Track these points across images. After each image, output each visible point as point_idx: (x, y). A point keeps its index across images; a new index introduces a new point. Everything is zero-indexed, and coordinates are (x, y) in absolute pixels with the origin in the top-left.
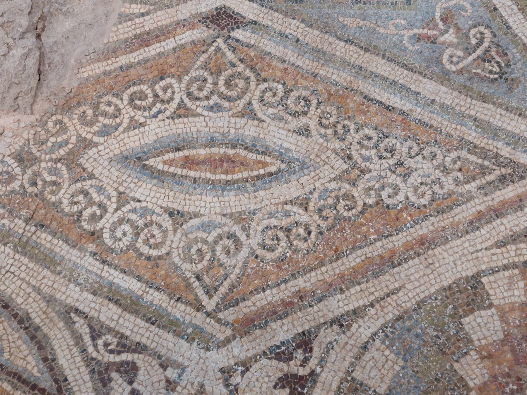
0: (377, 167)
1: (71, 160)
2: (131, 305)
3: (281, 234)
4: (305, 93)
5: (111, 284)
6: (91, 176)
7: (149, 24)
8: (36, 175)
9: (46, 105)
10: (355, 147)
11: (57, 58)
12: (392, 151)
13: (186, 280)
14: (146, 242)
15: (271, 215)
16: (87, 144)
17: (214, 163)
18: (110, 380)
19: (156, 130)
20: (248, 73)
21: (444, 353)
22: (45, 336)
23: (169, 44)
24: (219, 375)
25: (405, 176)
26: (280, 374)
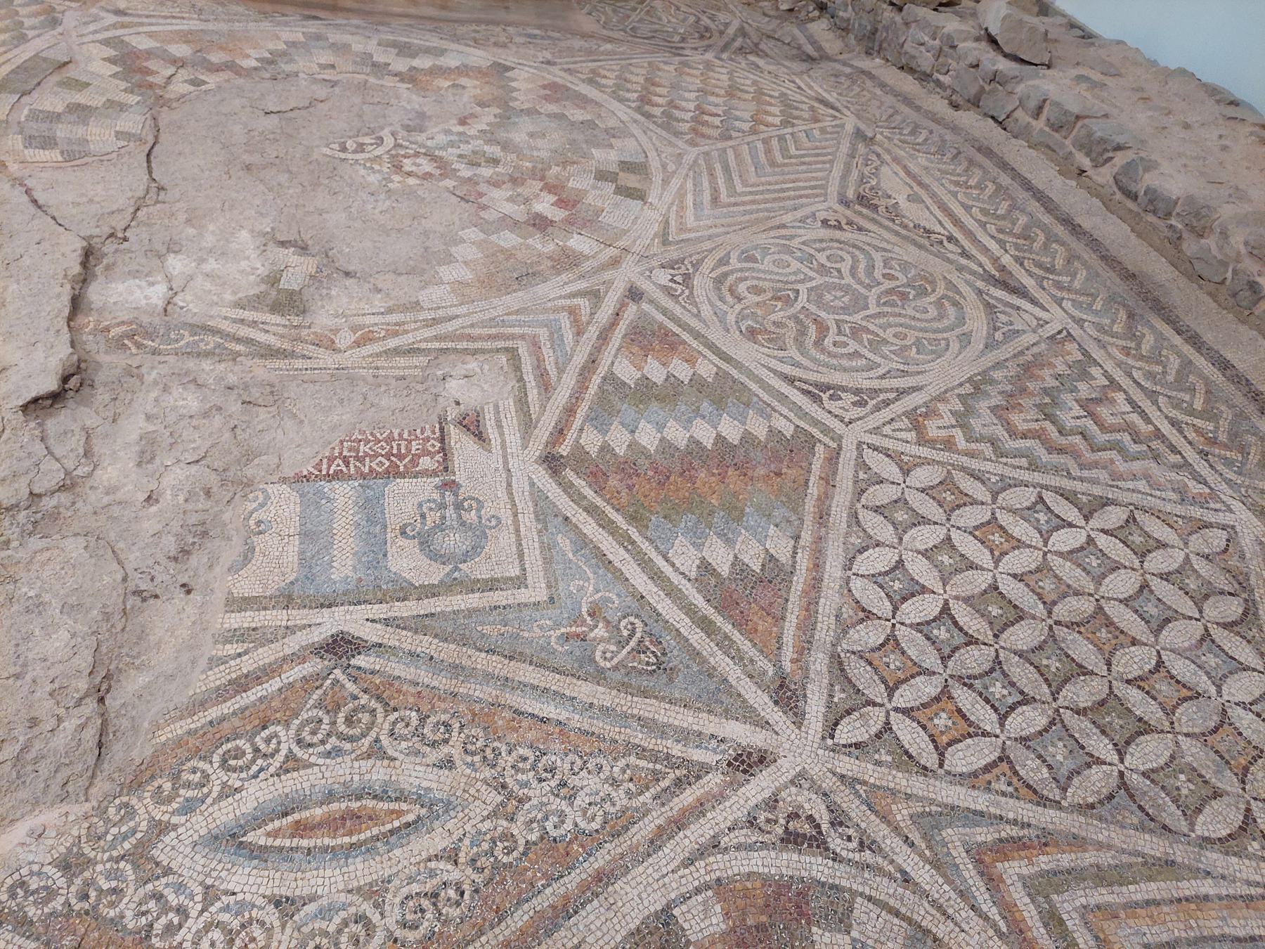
0: (537, 792)
1: (140, 856)
3: (425, 903)
4: (444, 717)
6: (168, 871)
7: (247, 665)
8: (88, 884)
9: (107, 786)
10: (509, 772)
11: (125, 723)
15: (411, 879)
16: (162, 829)
17: (333, 824)
19: (258, 793)
23: (275, 684)
25: (571, 798)
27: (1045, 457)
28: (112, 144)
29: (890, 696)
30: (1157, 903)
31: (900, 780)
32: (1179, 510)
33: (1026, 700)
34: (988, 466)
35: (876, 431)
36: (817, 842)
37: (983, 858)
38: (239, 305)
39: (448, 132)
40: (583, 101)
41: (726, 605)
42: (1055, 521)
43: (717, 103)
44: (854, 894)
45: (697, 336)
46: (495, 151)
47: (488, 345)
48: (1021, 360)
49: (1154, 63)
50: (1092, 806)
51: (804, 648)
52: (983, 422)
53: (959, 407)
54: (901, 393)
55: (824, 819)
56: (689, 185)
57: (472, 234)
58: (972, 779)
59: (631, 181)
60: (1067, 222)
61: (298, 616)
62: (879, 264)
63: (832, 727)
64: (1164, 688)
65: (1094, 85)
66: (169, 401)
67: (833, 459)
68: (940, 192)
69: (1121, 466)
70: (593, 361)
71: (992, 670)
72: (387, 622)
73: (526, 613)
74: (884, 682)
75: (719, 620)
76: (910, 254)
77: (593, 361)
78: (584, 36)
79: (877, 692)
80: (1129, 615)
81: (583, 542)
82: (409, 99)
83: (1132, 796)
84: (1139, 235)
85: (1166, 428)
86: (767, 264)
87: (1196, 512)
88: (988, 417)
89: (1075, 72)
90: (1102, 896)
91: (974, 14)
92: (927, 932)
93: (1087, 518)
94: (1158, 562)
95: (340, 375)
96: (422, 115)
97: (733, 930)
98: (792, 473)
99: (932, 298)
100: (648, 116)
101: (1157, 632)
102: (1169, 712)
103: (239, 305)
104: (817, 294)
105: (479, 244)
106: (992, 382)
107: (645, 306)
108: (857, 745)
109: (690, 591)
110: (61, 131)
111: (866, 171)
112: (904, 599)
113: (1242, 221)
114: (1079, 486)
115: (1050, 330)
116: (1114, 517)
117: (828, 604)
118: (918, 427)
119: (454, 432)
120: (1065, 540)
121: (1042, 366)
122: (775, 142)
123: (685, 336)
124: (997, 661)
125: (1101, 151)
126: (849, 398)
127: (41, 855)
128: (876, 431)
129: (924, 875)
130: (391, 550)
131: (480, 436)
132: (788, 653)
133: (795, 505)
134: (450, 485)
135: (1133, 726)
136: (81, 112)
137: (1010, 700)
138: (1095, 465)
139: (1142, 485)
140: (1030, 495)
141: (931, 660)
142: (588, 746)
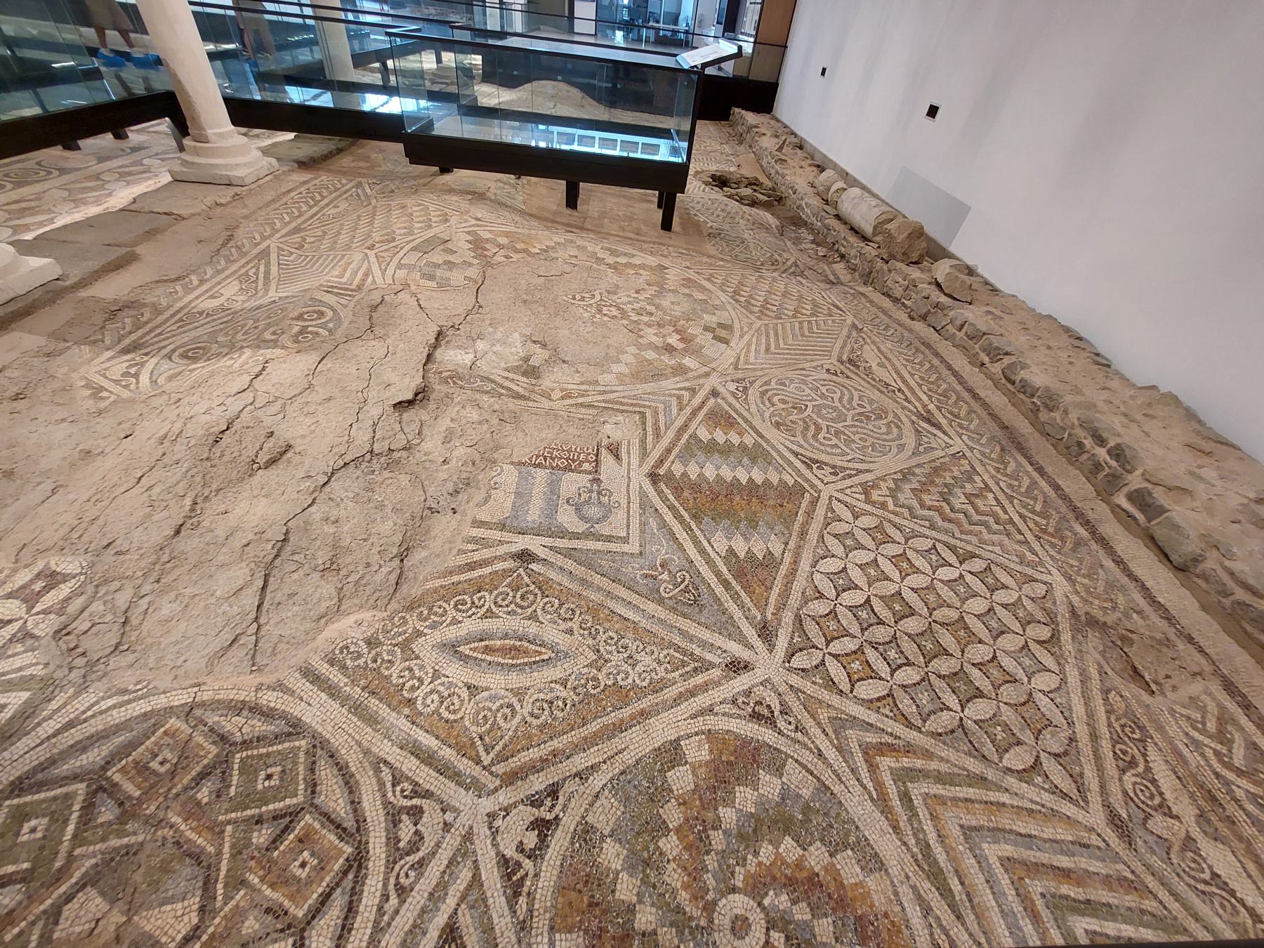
0: (616, 658)
1: (405, 646)
2: (427, 758)
3: (545, 706)
4: (572, 606)
5: (416, 741)
6: (417, 657)
7: (477, 557)
8: (377, 654)
9: (396, 606)
10: (602, 644)
11: (411, 575)
12: (626, 648)
13: (472, 739)
14: (447, 708)
15: (540, 691)
16: (419, 634)
17: (505, 651)
18: (400, 821)
19: (470, 626)
20: (537, 591)
21: (653, 801)
22: (357, 782)
23: (488, 570)
24: (486, 818)
25: (634, 666)
26: (532, 819)
27: (940, 523)
28: (461, 282)
29: (827, 645)
30: (972, 801)
31: (825, 695)
32: (1018, 568)
33: (909, 663)
34: (905, 522)
35: (841, 491)
36: (770, 721)
37: (871, 753)
38: (507, 370)
39: (629, 296)
40: (703, 289)
41: (740, 575)
42: (941, 561)
43: (776, 299)
44: (788, 756)
45: (746, 421)
46: (652, 309)
47: (631, 409)
48: (933, 465)
49: (1034, 310)
50: (940, 735)
51: (780, 608)
52: (906, 496)
53: (892, 485)
54: (859, 472)
55: (777, 709)
56: (754, 340)
57: (633, 350)
58: (868, 703)
59: (723, 333)
60: (970, 390)
61: (507, 536)
62: (856, 398)
63: (790, 656)
64: (995, 672)
65: (996, 317)
66: (464, 413)
67: (814, 502)
68: (898, 364)
69: (986, 536)
70: (685, 426)
71: (891, 642)
72: (551, 548)
73: (626, 557)
74: (824, 635)
75: (734, 583)
76: (876, 395)
77: (685, 426)
78: (709, 256)
79: (820, 641)
80: (980, 625)
81: (663, 525)
82: (612, 278)
83: (966, 734)
84: (1013, 405)
85: (1016, 518)
86: (792, 388)
87: (1029, 571)
88: (909, 494)
89: (986, 309)
90: (938, 790)
91: (930, 271)
92: (828, 788)
93: (961, 563)
94: (1000, 596)
95: (552, 414)
96: (617, 286)
97: (713, 760)
98: (790, 506)
99: (884, 422)
100: (737, 301)
101: (995, 638)
102: (997, 687)
103: (507, 370)
104: (818, 409)
105: (635, 355)
106: (914, 474)
107: (719, 400)
108: (803, 670)
109: (720, 563)
110: (439, 273)
111: (856, 346)
112: (844, 591)
113: (1078, 405)
114: (958, 543)
115: (952, 451)
116: (978, 565)
117: (799, 584)
118: (866, 493)
119: (604, 451)
120: (945, 573)
121: (945, 470)
122: (805, 324)
123: (739, 420)
124: (895, 637)
125: (996, 354)
126: (828, 470)
127: (359, 634)
128: (841, 491)
129: (831, 754)
130: (560, 510)
131: (617, 457)
132: (771, 609)
133: (788, 525)
134: (597, 481)
135: (972, 692)
136: (450, 265)
137: (899, 662)
138: (970, 533)
139: (997, 549)
140: (928, 544)
141: (855, 629)
142: (646, 638)
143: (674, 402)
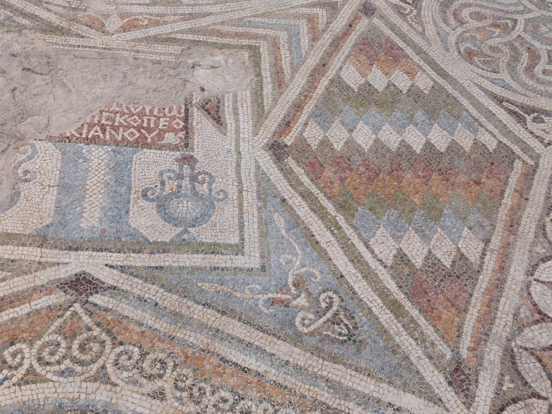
4: (161, 356)
20: (104, 336)
41: (416, 292)
45: (419, 52)
47: (234, 41)
51: (482, 338)
61: (50, 255)
67: (529, 174)
70: (323, 65)
72: (122, 269)
73: (241, 276)
75: (407, 305)
77: (323, 65)
81: (295, 222)
95: (106, 54)
98: (490, 183)
104: (533, 25)
107: (376, 21)
119: (197, 114)
123: (409, 51)
130: (133, 209)
131: (218, 121)
132: (466, 342)
133: (490, 212)
134: (189, 160)
143: (303, 27)
